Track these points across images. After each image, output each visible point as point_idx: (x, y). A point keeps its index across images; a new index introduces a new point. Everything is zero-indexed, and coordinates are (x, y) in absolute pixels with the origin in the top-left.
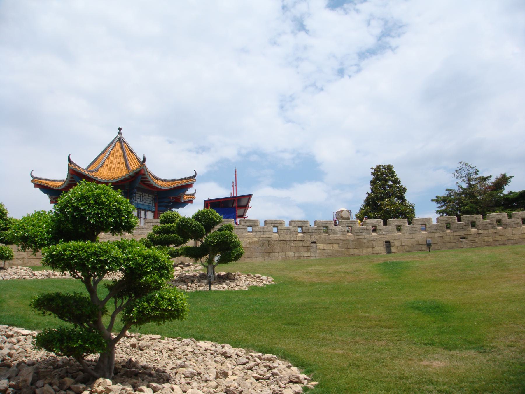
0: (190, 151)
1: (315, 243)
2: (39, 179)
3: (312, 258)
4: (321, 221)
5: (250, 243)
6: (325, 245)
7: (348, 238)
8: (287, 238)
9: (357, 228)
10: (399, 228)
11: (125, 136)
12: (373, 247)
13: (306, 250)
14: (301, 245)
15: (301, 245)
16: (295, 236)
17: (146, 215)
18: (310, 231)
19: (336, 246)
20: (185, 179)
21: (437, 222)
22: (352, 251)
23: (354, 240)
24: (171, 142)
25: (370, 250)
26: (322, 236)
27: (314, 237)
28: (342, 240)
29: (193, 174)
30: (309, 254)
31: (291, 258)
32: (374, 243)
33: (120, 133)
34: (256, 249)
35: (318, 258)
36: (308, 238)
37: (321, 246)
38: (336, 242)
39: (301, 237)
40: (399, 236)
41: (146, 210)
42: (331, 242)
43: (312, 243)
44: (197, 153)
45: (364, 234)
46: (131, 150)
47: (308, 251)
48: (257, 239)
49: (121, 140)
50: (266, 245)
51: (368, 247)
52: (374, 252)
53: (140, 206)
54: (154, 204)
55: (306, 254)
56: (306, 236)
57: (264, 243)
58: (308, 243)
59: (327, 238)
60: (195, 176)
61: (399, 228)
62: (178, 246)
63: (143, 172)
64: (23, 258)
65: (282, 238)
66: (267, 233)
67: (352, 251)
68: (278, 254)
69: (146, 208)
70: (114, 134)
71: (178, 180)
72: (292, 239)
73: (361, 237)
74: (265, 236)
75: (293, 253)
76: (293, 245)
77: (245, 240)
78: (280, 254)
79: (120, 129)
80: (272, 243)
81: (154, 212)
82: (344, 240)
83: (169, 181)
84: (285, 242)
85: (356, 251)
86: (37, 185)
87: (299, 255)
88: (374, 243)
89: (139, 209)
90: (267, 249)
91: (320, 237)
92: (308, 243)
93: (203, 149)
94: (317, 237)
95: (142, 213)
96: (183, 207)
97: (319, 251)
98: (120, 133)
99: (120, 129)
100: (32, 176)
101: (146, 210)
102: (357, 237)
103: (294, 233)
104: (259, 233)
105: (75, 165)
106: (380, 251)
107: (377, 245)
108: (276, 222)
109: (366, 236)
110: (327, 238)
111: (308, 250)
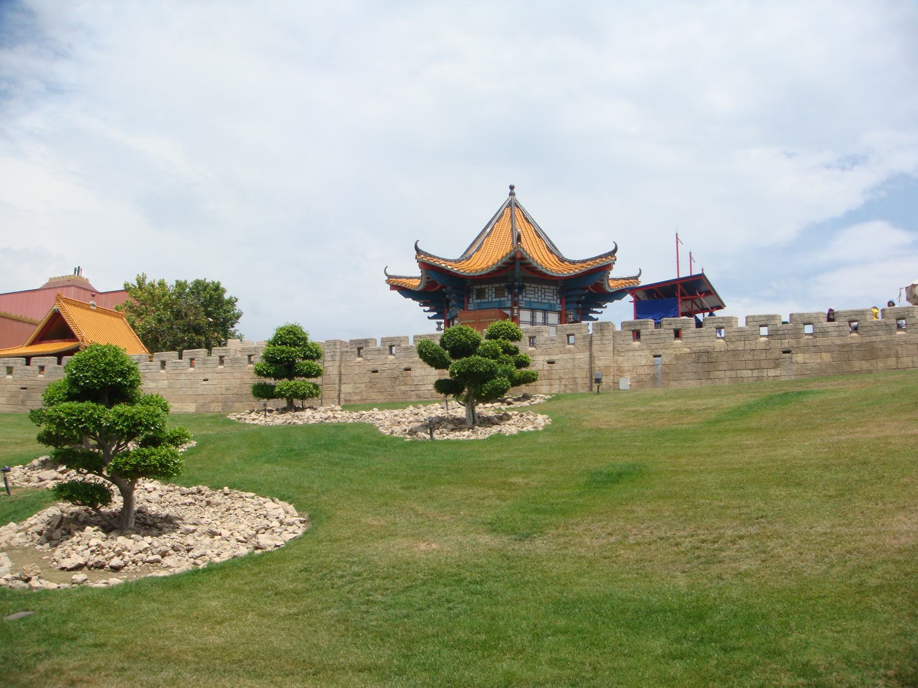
0: (828, 167)
1: (789, 352)
2: (396, 277)
3: (782, 379)
4: (800, 315)
5: (677, 357)
6: (807, 356)
7: (850, 341)
8: (740, 346)
9: (866, 324)
10: (677, 334)
11: (520, 198)
12: (897, 357)
13: (772, 365)
14: (763, 356)
15: (763, 356)
16: (753, 342)
17: (545, 318)
18: (780, 332)
19: (826, 357)
20: (601, 257)
21: (747, 323)
22: (857, 365)
23: (861, 345)
24: (790, 156)
25: (892, 362)
26: (802, 340)
27: (787, 343)
28: (838, 346)
29: (613, 248)
30: (778, 372)
31: (745, 380)
32: (899, 349)
33: (512, 194)
34: (688, 366)
35: (793, 378)
36: (778, 345)
37: (799, 358)
38: (828, 349)
39: (764, 343)
40: (901, 336)
41: (545, 311)
42: (818, 349)
43: (784, 352)
44: (843, 169)
45: (880, 333)
46: (526, 219)
47: (776, 366)
48: (688, 350)
49: (512, 204)
50: (704, 358)
51: (888, 356)
52: (899, 366)
53: (534, 306)
54: (559, 301)
55: (772, 373)
56: (773, 342)
57: (700, 356)
58: (777, 354)
59: (811, 344)
60: (615, 250)
61: (677, 334)
62: (277, 376)
63: (518, 256)
64: (361, 392)
65: (731, 347)
66: (706, 339)
67: (857, 365)
68: (723, 376)
69: (546, 307)
70: (505, 197)
71: (592, 259)
72: (748, 347)
73: (874, 339)
74: (701, 344)
75: (750, 372)
76: (750, 357)
77: (668, 352)
78: (728, 373)
79: (512, 188)
80: (715, 354)
81: (560, 313)
82: (843, 346)
83: (579, 262)
84: (735, 353)
85: (865, 365)
86: (394, 287)
87: (760, 374)
88: (899, 349)
89: (533, 310)
90: (705, 366)
91: (798, 343)
92: (777, 354)
93: (853, 161)
94: (793, 342)
95: (539, 316)
96: (620, 299)
97: (795, 367)
98: (512, 194)
99: (512, 188)
100: (387, 275)
101: (545, 311)
102: (868, 339)
103: (752, 337)
104: (693, 340)
105: (426, 254)
106: (911, 364)
107: (905, 352)
108: (721, 320)
109: (884, 338)
110: (811, 344)
111: (776, 364)
